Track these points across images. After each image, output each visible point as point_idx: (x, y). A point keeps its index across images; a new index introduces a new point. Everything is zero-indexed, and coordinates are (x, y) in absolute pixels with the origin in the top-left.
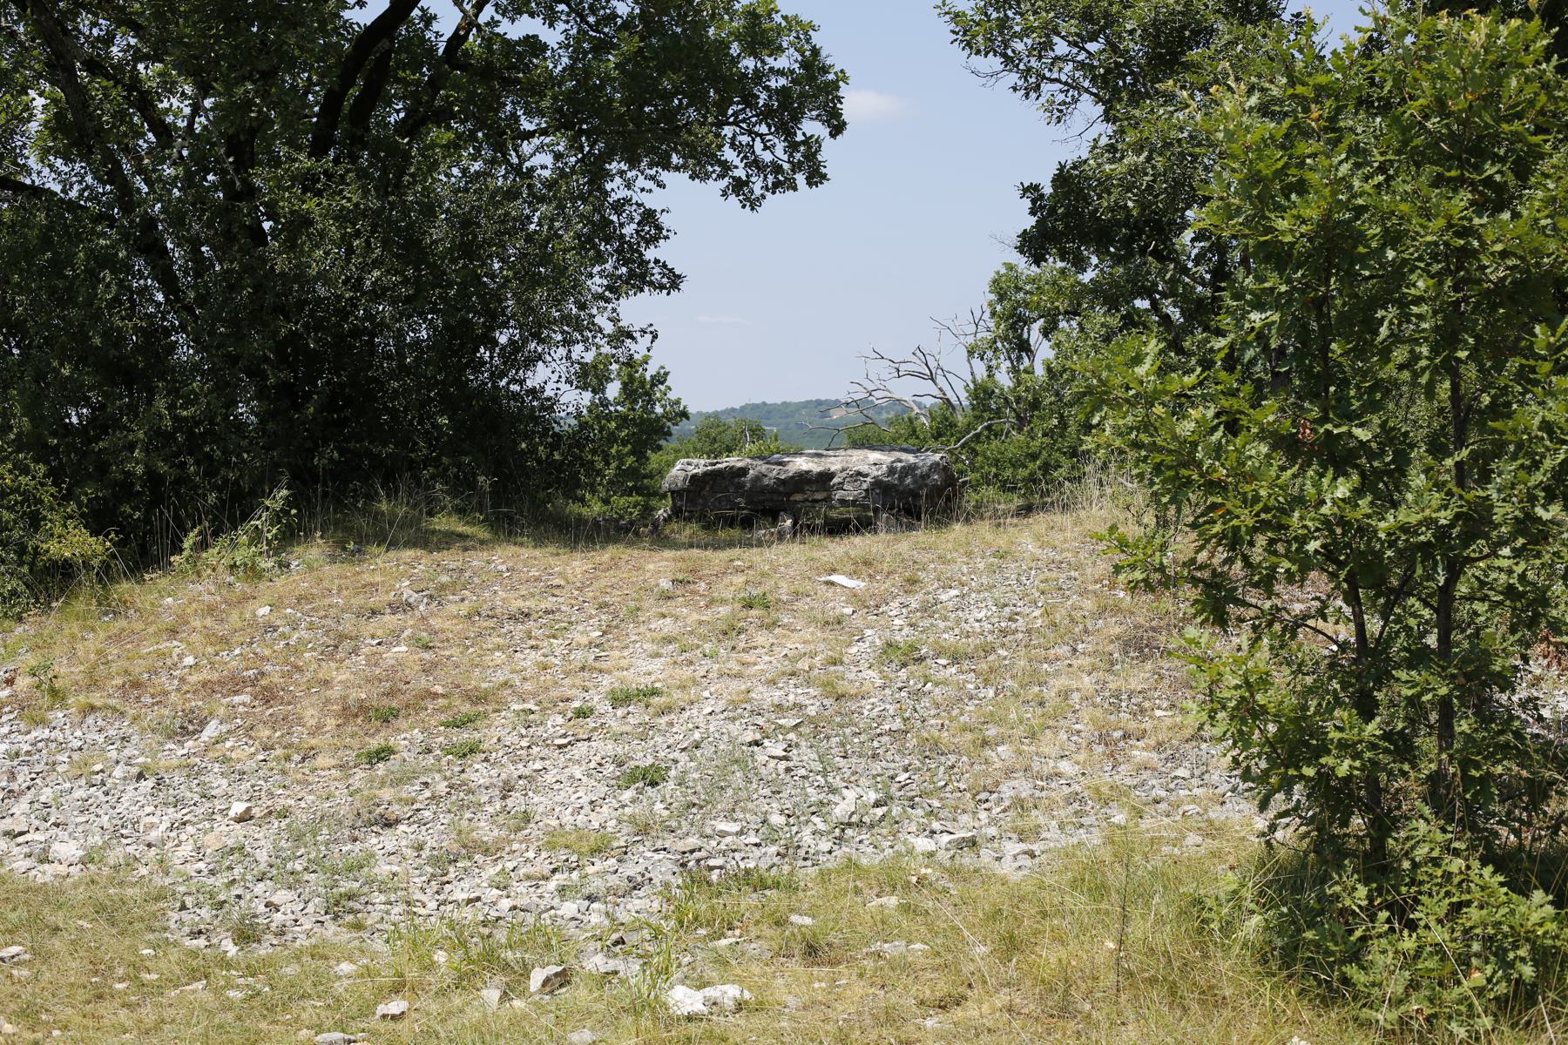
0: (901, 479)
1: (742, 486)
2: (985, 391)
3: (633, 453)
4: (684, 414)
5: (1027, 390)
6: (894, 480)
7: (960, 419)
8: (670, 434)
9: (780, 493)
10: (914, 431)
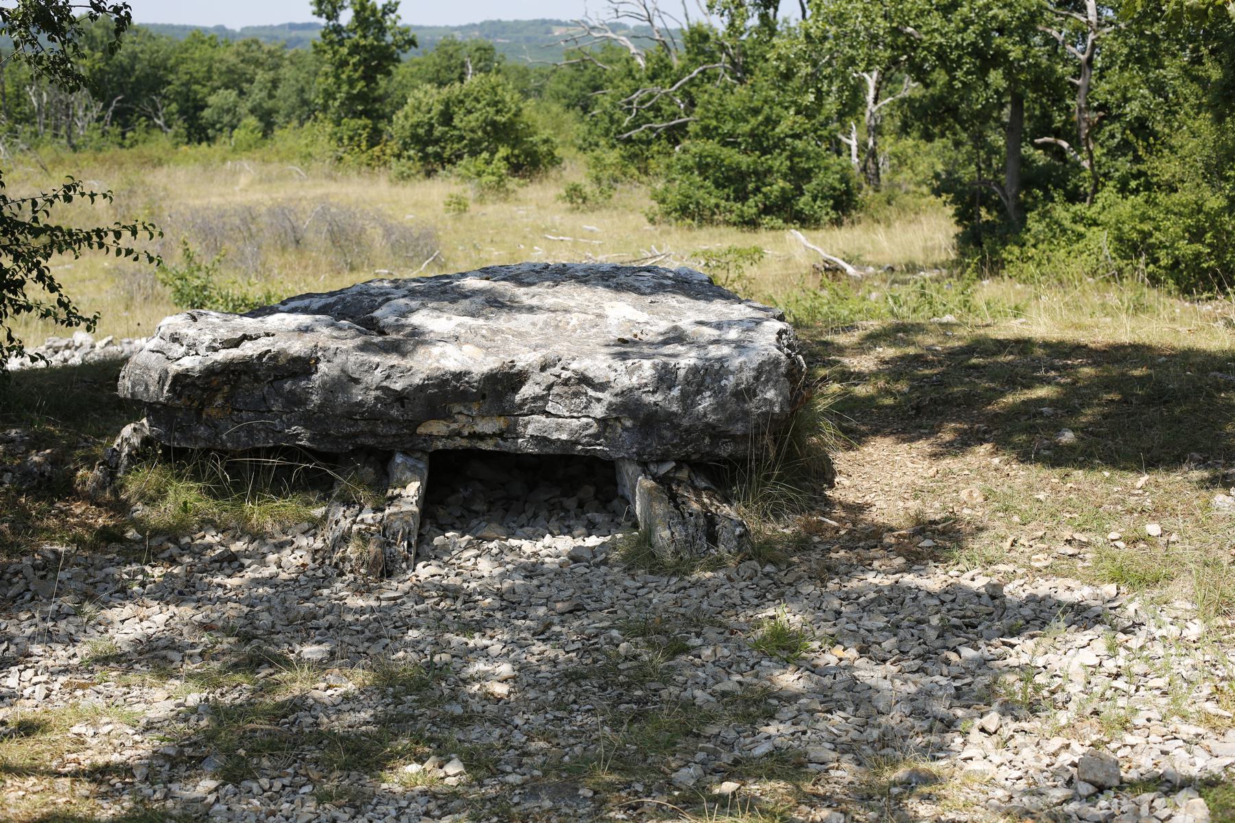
0: (687, 399)
1: (296, 400)
2: (700, 34)
3: (363, 78)
4: (412, 43)
5: (779, 58)
6: (668, 400)
7: (676, 63)
8: (399, 61)
9: (391, 421)
10: (630, 71)
